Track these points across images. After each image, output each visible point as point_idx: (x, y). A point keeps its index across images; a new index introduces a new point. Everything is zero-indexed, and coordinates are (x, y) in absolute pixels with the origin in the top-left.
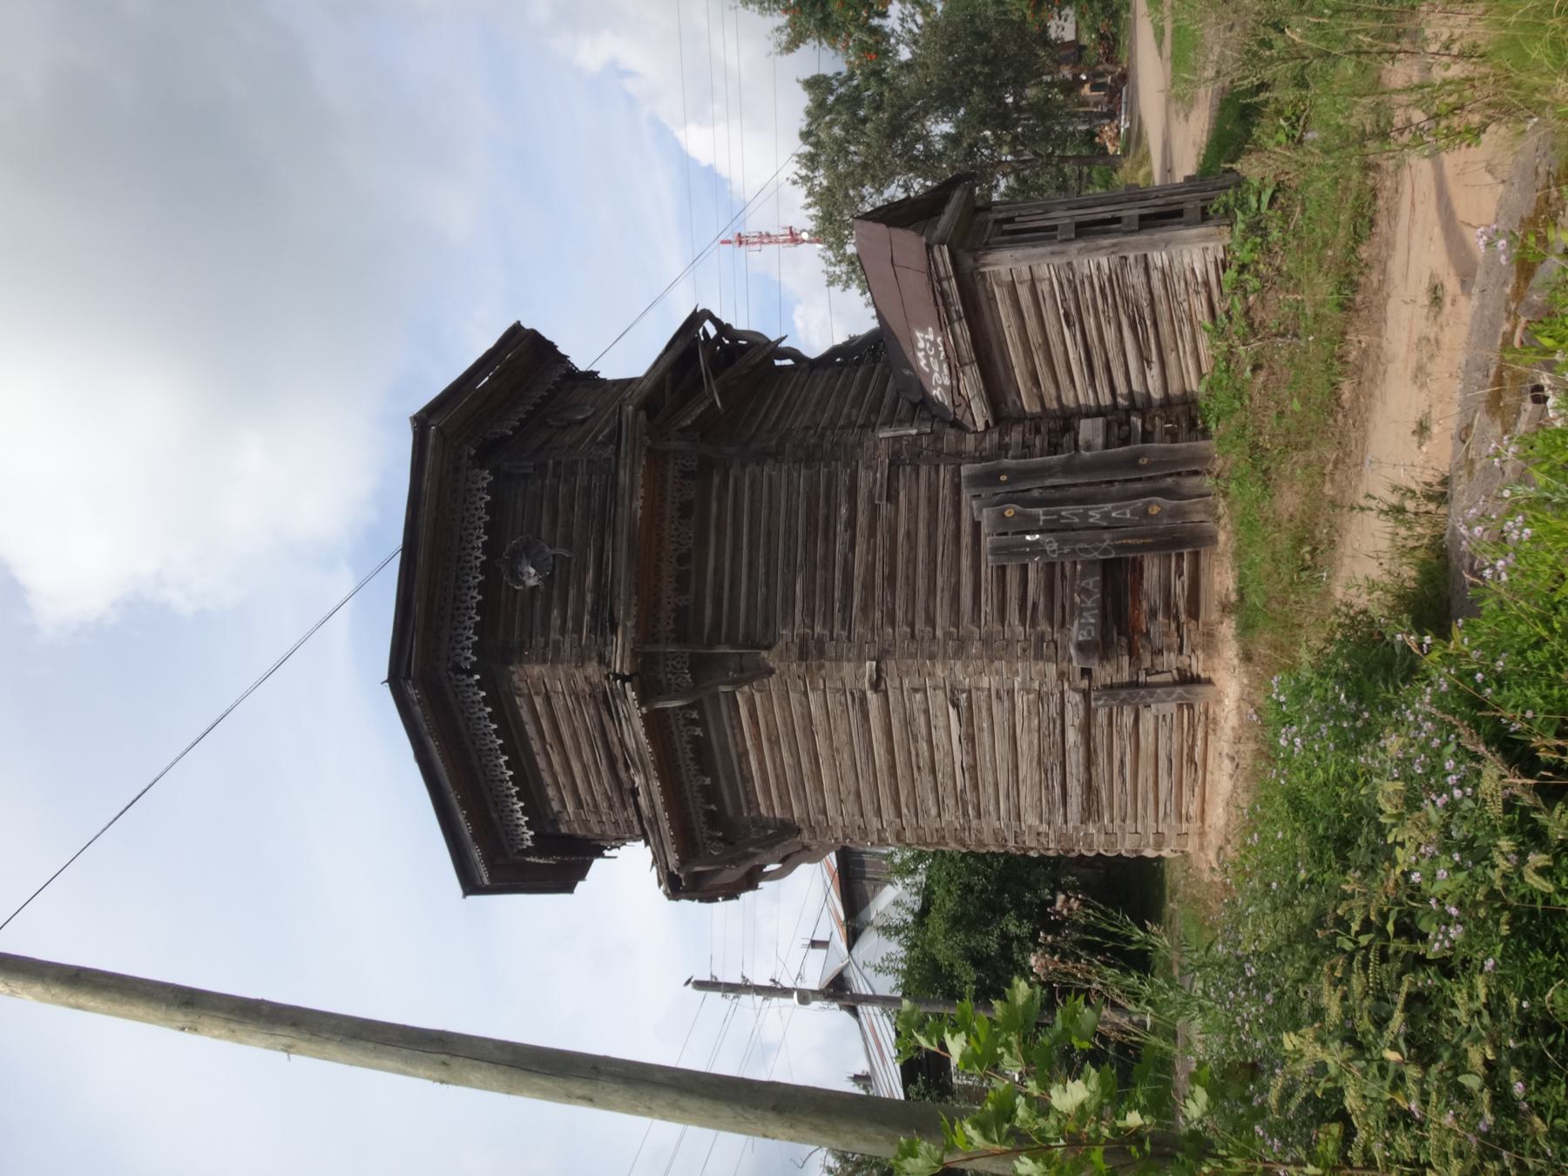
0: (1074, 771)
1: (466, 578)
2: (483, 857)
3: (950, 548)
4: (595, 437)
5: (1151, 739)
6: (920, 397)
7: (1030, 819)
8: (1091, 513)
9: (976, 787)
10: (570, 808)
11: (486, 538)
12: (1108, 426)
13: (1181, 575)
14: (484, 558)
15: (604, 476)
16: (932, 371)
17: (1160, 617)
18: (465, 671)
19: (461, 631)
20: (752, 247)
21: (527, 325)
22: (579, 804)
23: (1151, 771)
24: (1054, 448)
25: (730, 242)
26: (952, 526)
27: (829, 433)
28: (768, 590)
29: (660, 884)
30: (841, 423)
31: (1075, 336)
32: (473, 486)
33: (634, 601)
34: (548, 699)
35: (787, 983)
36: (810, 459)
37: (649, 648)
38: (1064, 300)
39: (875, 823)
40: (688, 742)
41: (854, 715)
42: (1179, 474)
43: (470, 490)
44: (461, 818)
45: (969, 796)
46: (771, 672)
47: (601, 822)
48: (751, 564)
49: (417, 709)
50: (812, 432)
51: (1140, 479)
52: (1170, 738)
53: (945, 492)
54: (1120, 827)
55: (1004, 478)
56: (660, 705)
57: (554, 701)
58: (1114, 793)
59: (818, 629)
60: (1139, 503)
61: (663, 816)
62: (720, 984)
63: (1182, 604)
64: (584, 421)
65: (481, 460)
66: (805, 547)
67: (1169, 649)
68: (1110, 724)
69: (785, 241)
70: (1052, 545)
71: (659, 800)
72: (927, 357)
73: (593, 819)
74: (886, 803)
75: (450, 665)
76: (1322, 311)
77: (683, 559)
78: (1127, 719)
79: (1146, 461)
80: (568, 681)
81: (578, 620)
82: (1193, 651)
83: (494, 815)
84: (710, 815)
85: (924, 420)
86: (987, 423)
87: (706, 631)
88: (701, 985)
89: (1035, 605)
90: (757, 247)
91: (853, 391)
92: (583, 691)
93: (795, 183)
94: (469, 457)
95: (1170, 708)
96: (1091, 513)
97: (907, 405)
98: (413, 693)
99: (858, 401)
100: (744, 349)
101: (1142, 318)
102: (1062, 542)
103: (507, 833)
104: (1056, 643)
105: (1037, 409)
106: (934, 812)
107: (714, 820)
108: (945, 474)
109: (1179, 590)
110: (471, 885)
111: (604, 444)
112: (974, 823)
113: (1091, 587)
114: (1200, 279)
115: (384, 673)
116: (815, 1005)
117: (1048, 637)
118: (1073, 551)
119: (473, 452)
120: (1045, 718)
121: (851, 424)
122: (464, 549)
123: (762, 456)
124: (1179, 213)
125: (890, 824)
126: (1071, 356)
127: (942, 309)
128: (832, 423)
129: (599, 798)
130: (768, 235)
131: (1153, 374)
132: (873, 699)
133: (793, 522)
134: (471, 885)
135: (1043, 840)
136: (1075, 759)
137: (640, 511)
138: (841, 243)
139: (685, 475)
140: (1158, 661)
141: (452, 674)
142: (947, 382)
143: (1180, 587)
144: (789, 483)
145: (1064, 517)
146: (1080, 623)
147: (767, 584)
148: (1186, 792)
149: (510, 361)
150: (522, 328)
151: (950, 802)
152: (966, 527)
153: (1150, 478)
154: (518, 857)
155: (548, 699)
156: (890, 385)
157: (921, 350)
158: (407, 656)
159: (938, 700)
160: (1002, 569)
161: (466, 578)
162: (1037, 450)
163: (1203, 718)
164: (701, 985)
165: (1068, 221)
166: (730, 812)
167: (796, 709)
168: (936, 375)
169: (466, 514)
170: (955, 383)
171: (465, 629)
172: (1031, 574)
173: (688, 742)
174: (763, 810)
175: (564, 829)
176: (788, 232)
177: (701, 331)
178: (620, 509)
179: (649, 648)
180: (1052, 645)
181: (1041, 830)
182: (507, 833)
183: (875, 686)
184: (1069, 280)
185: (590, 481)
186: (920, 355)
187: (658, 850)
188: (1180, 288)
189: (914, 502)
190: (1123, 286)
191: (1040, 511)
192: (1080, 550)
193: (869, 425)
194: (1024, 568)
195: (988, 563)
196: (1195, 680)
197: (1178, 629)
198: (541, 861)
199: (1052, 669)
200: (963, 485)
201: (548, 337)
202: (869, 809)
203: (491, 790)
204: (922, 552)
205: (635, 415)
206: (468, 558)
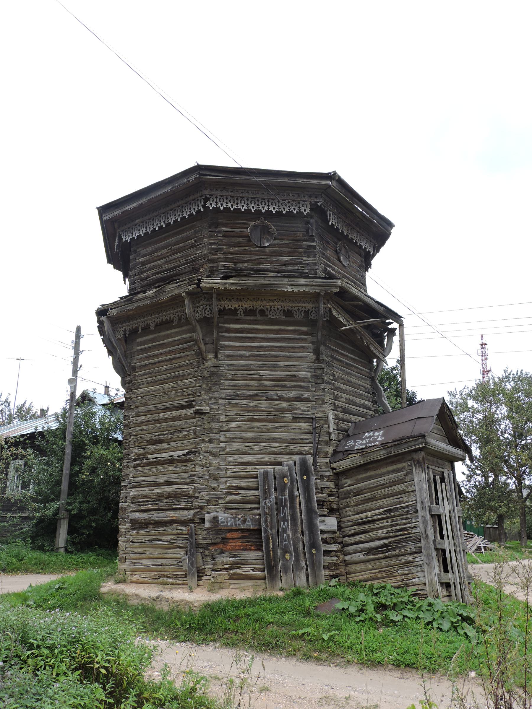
0: (155, 515)
1: (253, 202)
2: (116, 216)
3: (268, 450)
4: (330, 267)
5: (171, 555)
6: (351, 434)
7: (133, 493)
8: (286, 523)
9: (148, 464)
10: (141, 260)
11: (274, 212)
12: (334, 532)
15: (307, 271)
16: (362, 440)
17: (231, 560)
18: (205, 204)
19: (225, 201)
21: (393, 231)
22: (143, 264)
24: (321, 504)
25: (482, 339)
26: (280, 451)
27: (331, 387)
28: (247, 357)
29: (102, 305)
30: (337, 393)
31: (380, 515)
32: (301, 205)
33: (238, 288)
34: (193, 246)
35: (79, 374)
36: (316, 377)
37: (215, 296)
39: (133, 414)
40: (170, 318)
41: (183, 402)
42: (307, 570)
43: (299, 203)
45: (144, 461)
47: (135, 275)
48: (261, 347)
50: (331, 378)
51: (304, 549)
52: (171, 565)
54: (128, 540)
55: (305, 477)
56: (186, 301)
57: (192, 249)
58: (144, 535)
61: (134, 306)
62: (79, 339)
63: (238, 571)
64: (339, 260)
65: (315, 208)
66: (270, 375)
67: (215, 564)
68: (178, 534)
69: (483, 368)
71: (141, 304)
72: (370, 437)
73: (136, 271)
74: (142, 419)
75: (208, 196)
76: (278, 643)
77: (262, 312)
78: (180, 543)
79: (314, 552)
80: (201, 256)
81: (232, 260)
82: (213, 577)
83: (137, 221)
85: (338, 436)
86: (335, 469)
87: (226, 325)
90: (480, 354)
91: (356, 400)
92: (196, 264)
93: (505, 371)
95: (186, 566)
96: (286, 523)
97: (346, 427)
98: (193, 178)
99: (349, 402)
100: (381, 343)
102: (271, 508)
103: (129, 228)
104: (217, 505)
107: (134, 332)
109: (245, 569)
110: (103, 210)
111: (325, 271)
112: (132, 464)
113: (247, 523)
114: (408, 582)
115: (202, 163)
116: (68, 388)
117: (220, 501)
118: (265, 514)
120: (181, 500)
121: (336, 398)
122: (268, 201)
123: (317, 352)
124: (446, 570)
125: (132, 421)
126: (370, 513)
127: (391, 444)
128: (337, 389)
129: (146, 274)
130: (486, 359)
131: (360, 557)
133: (283, 369)
134: (103, 210)
135: (123, 500)
137: (285, 290)
138: (475, 398)
139: (307, 313)
140: (209, 559)
142: (356, 448)
143: (246, 570)
144: (304, 366)
145: (284, 509)
146: (228, 518)
148: (145, 574)
149: (372, 222)
150: (392, 228)
152: (279, 458)
153: (305, 555)
155: (193, 246)
157: (374, 434)
158: (212, 174)
161: (253, 202)
162: (320, 495)
163: (180, 582)
164: (78, 329)
165: (442, 511)
166: (138, 340)
168: (360, 442)
169: (287, 201)
170: (355, 452)
171: (227, 203)
173: (170, 318)
176: (489, 369)
177: (390, 321)
178: (286, 279)
179: (215, 296)
180: (217, 503)
181: (128, 498)
182: (129, 228)
183: (197, 412)
184: (408, 511)
185: (304, 264)
186: (371, 434)
187: (118, 304)
188: (405, 571)
189: (293, 431)
190: (405, 540)
191: (287, 496)
192: (266, 517)
193: (335, 408)
194: (257, 489)
195: (260, 470)
197: (225, 569)
200: (301, 456)
201: (387, 242)
203: (149, 219)
204: (266, 435)
205: (336, 286)
206: (263, 203)
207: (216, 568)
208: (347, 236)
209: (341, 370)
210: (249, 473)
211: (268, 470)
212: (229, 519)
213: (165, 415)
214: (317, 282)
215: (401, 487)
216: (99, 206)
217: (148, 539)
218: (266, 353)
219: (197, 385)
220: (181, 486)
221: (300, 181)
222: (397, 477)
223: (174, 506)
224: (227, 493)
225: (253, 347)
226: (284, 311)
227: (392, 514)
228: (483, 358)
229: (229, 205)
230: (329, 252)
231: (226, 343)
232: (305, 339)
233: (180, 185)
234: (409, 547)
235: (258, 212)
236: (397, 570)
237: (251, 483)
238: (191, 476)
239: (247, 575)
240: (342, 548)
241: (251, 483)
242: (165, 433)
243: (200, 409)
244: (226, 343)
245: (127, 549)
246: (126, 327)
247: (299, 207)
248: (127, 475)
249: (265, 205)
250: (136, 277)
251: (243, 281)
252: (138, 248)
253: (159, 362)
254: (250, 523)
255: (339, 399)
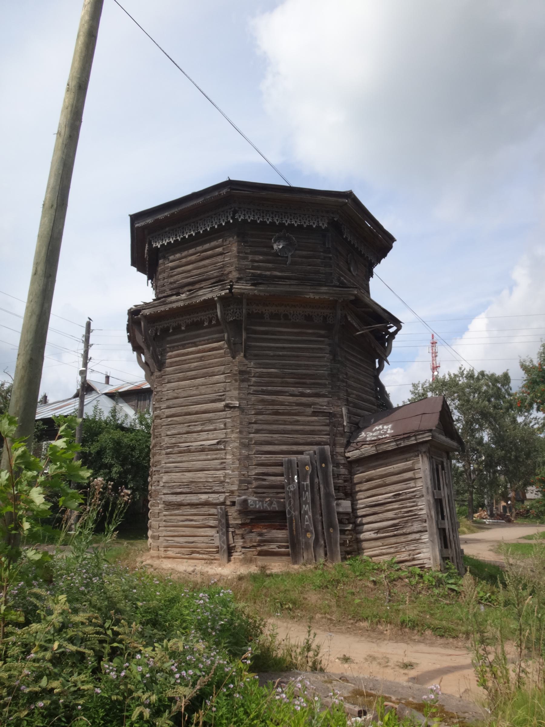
0: (188, 498)
1: (277, 216)
2: (148, 224)
4: (343, 276)
5: (203, 534)
6: (361, 427)
7: (166, 478)
8: (307, 506)
9: (180, 452)
10: (170, 264)
13: (279, 547)
14: (287, 224)
15: (324, 280)
16: (373, 432)
17: (259, 538)
19: (253, 214)
20: (430, 349)
21: (394, 244)
22: (172, 269)
23: (188, 533)
24: (337, 489)
25: (433, 338)
26: (301, 441)
27: (344, 384)
28: (272, 356)
29: (135, 306)
30: (349, 390)
31: (389, 498)
32: (319, 220)
33: (266, 294)
34: (221, 254)
35: (89, 365)
37: (244, 301)
38: (406, 493)
39: (164, 406)
40: (201, 319)
41: (213, 396)
42: (325, 547)
44: (166, 214)
45: (176, 449)
46: (234, 357)
47: (164, 278)
48: (284, 348)
49: (217, 193)
50: (345, 377)
51: (323, 528)
52: (203, 543)
53: (317, 438)
58: (178, 516)
59: (253, 379)
60: (312, 528)
62: (89, 334)
63: (265, 548)
64: (350, 271)
66: (292, 373)
67: (244, 542)
69: (433, 364)
70: (293, 487)
71: (174, 305)
72: (380, 430)
73: (165, 275)
74: (173, 411)
75: (237, 209)
77: (286, 316)
78: (212, 523)
79: (332, 531)
80: (229, 263)
82: (243, 553)
83: (167, 229)
84: (168, 329)
86: (349, 457)
87: (253, 327)
88: (88, 325)
89: (264, 480)
90: (431, 351)
92: (225, 271)
93: (460, 368)
94: (333, 218)
96: (307, 506)
98: (224, 191)
99: (359, 398)
101: (398, 530)
102: (294, 493)
103: (159, 235)
104: (247, 489)
105: (355, 481)
106: (169, 433)
107: (165, 331)
108: (325, 438)
109: (272, 547)
110: (135, 218)
111: (339, 280)
112: (164, 452)
113: (273, 506)
116: (79, 378)
117: (250, 486)
118: (290, 498)
119: (335, 219)
120: (212, 485)
121: (348, 394)
122: (291, 215)
123: (333, 353)
124: (446, 547)
126: (380, 497)
127: (402, 437)
128: (349, 386)
129: (175, 278)
130: (436, 356)
132: (221, 405)
135: (156, 484)
136: (193, 499)
137: (308, 297)
138: (432, 390)
139: (325, 318)
141: (232, 210)
142: (368, 439)
143: (273, 547)
144: (321, 366)
145: (305, 493)
146: (256, 501)
147: (274, 356)
149: (378, 236)
150: (393, 242)
151: (173, 440)
152: (301, 448)
153: (323, 533)
154: (148, 240)
155: (221, 254)
156: (367, 413)
157: (383, 427)
158: (241, 189)
159: (221, 435)
160: (281, 465)
161: (277, 216)
162: (337, 481)
163: (212, 558)
164: (88, 325)
165: (443, 495)
166: (169, 339)
167: (216, 369)
168: (371, 434)
169: (307, 216)
170: (368, 443)
171: (254, 216)
172: (279, 478)
173: (201, 319)
174: (170, 354)
175: (161, 261)
176: (438, 365)
177: (392, 325)
179: (244, 301)
181: (161, 482)
183: (227, 406)
184: (415, 495)
185: (322, 273)
186: (381, 427)
188: (412, 547)
190: (413, 521)
191: (308, 482)
194: (282, 475)
195: (284, 458)
196: (230, 554)
197: (254, 546)
198: (146, 251)
199: (235, 488)
200: (320, 446)
201: (389, 254)
202: (170, 403)
203: (179, 228)
204: (289, 427)
206: (286, 217)
207: (245, 545)
208: (357, 248)
209: (352, 369)
210: (274, 461)
211: (292, 458)
212: (257, 502)
213: (195, 408)
214: (335, 290)
215: (409, 475)
216: (395, 242)
217: (181, 519)
218: (289, 353)
219: (227, 381)
220: (213, 472)
221: (321, 198)
222: (405, 465)
223: (206, 490)
224: (256, 479)
225: (277, 348)
226: (305, 315)
227: (401, 498)
228: (434, 355)
229: (256, 217)
230: (342, 263)
231: (253, 344)
232: (323, 341)
233: (211, 198)
234: (415, 526)
235: (282, 225)
236: (404, 547)
237: (278, 469)
238: (222, 463)
239: (273, 552)
240: (355, 527)
241: (278, 469)
242: (196, 423)
243: (230, 403)
244: (253, 344)
245: (160, 528)
246: (158, 327)
247: (318, 222)
248: (159, 462)
249: (241, 213)
250: (166, 280)
251: (271, 288)
252: (170, 256)
253: (189, 359)
254: (276, 506)
255: (351, 396)
